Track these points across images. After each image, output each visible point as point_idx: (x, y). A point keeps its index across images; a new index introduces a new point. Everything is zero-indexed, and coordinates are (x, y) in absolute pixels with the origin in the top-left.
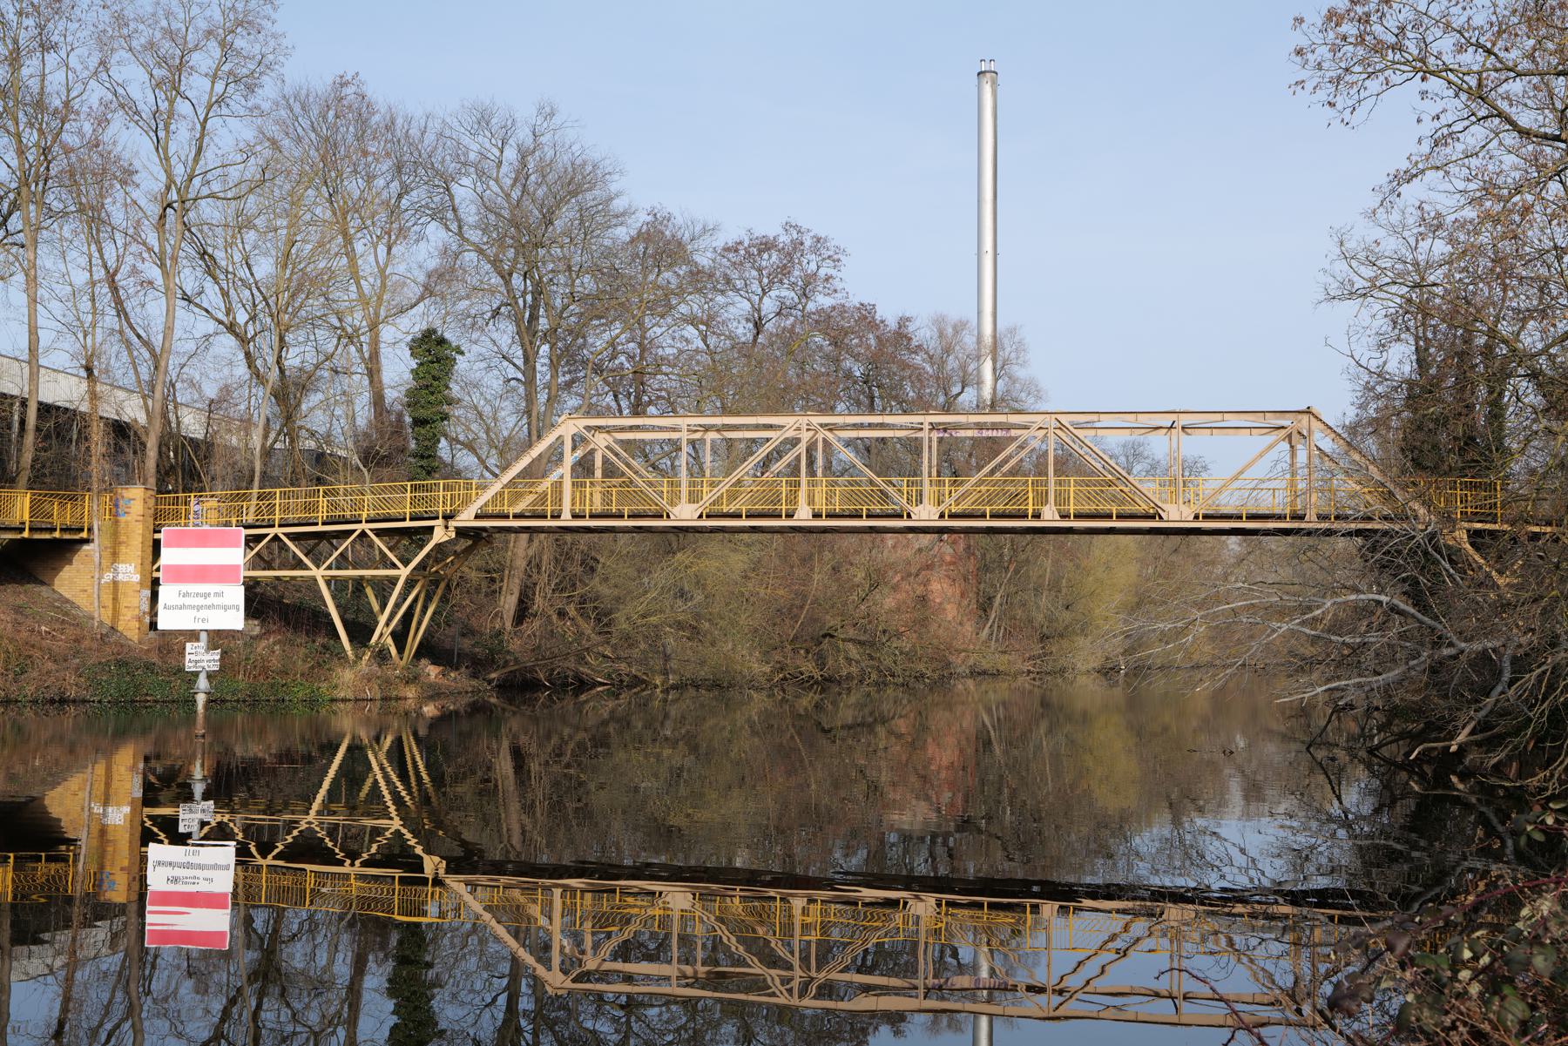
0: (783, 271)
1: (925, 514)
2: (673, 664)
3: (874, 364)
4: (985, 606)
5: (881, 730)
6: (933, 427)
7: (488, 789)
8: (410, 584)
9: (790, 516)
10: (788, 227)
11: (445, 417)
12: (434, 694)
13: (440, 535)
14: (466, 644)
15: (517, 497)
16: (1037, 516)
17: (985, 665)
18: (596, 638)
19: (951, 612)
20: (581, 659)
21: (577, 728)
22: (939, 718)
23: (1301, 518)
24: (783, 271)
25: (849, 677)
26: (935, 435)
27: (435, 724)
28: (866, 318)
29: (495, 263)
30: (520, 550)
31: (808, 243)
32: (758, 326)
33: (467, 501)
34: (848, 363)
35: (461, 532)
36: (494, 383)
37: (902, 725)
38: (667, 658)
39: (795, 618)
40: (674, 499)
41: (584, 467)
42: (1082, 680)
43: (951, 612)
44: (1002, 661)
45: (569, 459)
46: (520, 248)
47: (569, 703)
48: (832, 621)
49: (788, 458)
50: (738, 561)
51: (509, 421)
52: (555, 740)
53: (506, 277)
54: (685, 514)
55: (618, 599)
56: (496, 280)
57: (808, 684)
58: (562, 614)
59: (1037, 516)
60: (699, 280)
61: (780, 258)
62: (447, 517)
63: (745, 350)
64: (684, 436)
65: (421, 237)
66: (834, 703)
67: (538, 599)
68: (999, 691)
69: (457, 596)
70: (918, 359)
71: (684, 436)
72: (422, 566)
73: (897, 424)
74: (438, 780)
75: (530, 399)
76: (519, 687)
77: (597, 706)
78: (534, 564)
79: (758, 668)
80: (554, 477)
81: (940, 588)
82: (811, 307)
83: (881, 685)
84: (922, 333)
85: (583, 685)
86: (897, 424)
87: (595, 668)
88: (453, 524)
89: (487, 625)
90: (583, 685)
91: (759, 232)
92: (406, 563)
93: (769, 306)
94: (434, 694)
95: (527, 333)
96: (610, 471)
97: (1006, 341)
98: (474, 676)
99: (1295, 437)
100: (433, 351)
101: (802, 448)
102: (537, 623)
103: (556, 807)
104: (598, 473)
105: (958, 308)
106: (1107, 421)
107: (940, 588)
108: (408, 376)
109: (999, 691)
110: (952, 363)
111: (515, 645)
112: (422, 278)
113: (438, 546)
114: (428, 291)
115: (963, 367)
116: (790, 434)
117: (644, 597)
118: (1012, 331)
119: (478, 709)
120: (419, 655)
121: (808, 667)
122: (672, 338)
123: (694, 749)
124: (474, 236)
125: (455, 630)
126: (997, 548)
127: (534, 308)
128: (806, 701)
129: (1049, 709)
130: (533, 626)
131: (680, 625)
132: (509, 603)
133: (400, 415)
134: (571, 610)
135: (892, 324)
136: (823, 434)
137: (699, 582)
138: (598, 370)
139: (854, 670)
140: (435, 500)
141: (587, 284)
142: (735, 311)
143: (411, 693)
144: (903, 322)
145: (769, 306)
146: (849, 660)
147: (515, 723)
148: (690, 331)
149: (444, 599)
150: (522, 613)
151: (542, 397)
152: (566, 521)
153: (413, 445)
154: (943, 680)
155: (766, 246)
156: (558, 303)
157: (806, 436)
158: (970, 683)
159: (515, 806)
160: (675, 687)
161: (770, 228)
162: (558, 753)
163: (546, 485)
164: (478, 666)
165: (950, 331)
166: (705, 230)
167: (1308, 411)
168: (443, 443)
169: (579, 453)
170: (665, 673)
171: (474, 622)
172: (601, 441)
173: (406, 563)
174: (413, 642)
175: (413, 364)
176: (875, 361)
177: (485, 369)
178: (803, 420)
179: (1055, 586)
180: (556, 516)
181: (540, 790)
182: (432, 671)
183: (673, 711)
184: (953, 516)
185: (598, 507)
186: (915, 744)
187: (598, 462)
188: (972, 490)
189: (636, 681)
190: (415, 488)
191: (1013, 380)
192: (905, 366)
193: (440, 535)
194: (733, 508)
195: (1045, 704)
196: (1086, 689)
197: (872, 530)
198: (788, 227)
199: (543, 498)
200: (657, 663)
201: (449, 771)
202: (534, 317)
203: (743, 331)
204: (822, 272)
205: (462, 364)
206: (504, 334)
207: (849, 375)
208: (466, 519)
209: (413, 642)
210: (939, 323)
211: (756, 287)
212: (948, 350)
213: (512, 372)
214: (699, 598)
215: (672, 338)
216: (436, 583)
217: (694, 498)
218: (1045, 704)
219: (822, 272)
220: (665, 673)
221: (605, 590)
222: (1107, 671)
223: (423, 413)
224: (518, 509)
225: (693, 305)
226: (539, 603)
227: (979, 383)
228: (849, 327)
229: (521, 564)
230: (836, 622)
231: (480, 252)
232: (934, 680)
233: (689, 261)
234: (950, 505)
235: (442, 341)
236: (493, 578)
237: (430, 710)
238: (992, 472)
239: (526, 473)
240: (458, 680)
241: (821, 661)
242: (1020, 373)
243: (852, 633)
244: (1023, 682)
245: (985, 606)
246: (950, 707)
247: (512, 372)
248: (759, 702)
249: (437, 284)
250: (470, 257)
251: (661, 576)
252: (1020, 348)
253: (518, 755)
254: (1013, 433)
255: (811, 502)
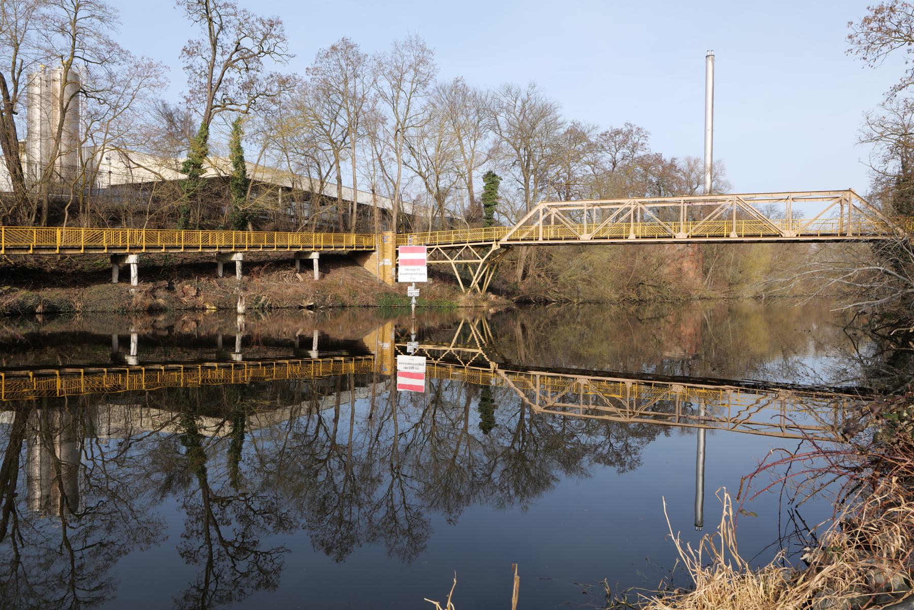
0: (625, 142)
1: (681, 236)
2: (581, 294)
3: (662, 177)
4: (705, 272)
5: (662, 320)
6: (685, 202)
7: (512, 340)
8: (484, 265)
9: (626, 238)
10: (627, 124)
11: (496, 204)
12: (493, 305)
13: (495, 247)
14: (504, 287)
15: (523, 232)
16: (728, 236)
17: (705, 295)
18: (552, 285)
19: (691, 274)
20: (546, 292)
21: (545, 318)
22: (686, 316)
23: (845, 235)
24: (625, 142)
25: (650, 300)
26: (686, 205)
27: (493, 316)
28: (658, 159)
29: (514, 145)
30: (524, 252)
31: (634, 130)
32: (614, 164)
33: (504, 235)
34: (650, 177)
35: (502, 246)
36: (513, 190)
37: (671, 318)
38: (579, 292)
39: (628, 277)
40: (581, 232)
41: (547, 221)
42: (746, 301)
43: (691, 274)
44: (713, 294)
45: (542, 218)
46: (523, 139)
47: (542, 308)
48: (643, 278)
49: (626, 215)
50: (606, 255)
51: (519, 205)
52: (537, 322)
53: (518, 150)
54: (585, 238)
55: (560, 270)
56: (514, 151)
57: (633, 302)
58: (539, 276)
59: (728, 236)
60: (591, 147)
61: (622, 137)
62: (497, 241)
63: (609, 174)
64: (585, 208)
65: (486, 137)
66: (644, 310)
67: (530, 270)
68: (711, 305)
69: (501, 269)
70: (679, 175)
71: (585, 208)
72: (488, 259)
73: (670, 201)
74: (495, 335)
75: (527, 196)
76: (524, 303)
77: (552, 310)
78: (529, 257)
79: (614, 296)
80: (536, 225)
81: (687, 265)
82: (636, 156)
83: (662, 303)
84: (681, 164)
85: (547, 302)
86: (670, 201)
87: (551, 296)
88: (499, 243)
89: (512, 280)
90: (547, 302)
91: (615, 127)
92: (483, 257)
93: (619, 156)
94: (493, 305)
95: (526, 171)
96: (557, 222)
97: (716, 166)
98: (507, 299)
99: (843, 201)
100: (491, 179)
101: (631, 212)
102: (530, 279)
103: (538, 346)
104: (553, 223)
105: (695, 152)
106: (759, 197)
107: (687, 265)
108: (482, 189)
109: (711, 305)
110: (693, 176)
111: (522, 287)
112: (487, 152)
113: (494, 251)
114: (489, 157)
115: (698, 177)
116: (627, 206)
117: (571, 270)
118: (719, 162)
119: (508, 310)
120: (487, 291)
121: (634, 296)
122: (581, 170)
123: (589, 326)
124: (506, 135)
125: (500, 282)
126: (711, 249)
127: (528, 161)
128: (632, 309)
129: (732, 312)
130: (528, 280)
131: (584, 280)
132: (520, 272)
133: (480, 204)
134: (543, 274)
135: (669, 161)
136: (640, 206)
137: (591, 264)
138: (552, 184)
139: (652, 297)
140: (492, 235)
141: (548, 151)
142: (605, 159)
143: (485, 304)
144: (673, 160)
145: (619, 156)
146: (650, 293)
147: (522, 316)
148: (588, 168)
149: (496, 271)
150: (524, 276)
151: (531, 195)
152: (541, 241)
153: (484, 214)
154: (688, 301)
155: (618, 132)
156: (537, 159)
157: (633, 207)
158: (699, 302)
159: (522, 346)
160: (582, 303)
161: (620, 125)
162: (538, 327)
163: (533, 228)
164: (509, 295)
165: (692, 163)
166: (593, 128)
167: (850, 190)
168: (495, 213)
169: (545, 216)
170: (578, 298)
171: (507, 279)
172: (553, 211)
173: (483, 257)
174: (485, 286)
175: (484, 184)
176: (661, 176)
177: (511, 185)
178: (632, 201)
179: (735, 264)
180: (537, 240)
181: (532, 338)
182: (492, 297)
183: (581, 312)
184: (692, 237)
185: (553, 236)
186: (676, 326)
187: (553, 219)
188: (701, 227)
189: (567, 301)
190: (485, 230)
191: (719, 181)
192: (674, 177)
193: (495, 247)
194: (604, 235)
195: (730, 310)
196: (747, 304)
197: (659, 243)
198: (627, 124)
199: (532, 233)
200: (575, 294)
201: (499, 333)
202: (528, 165)
203: (609, 166)
204: (640, 142)
205: (502, 183)
206: (517, 171)
207: (651, 182)
208: (504, 241)
209: (485, 286)
210: (688, 160)
211: (613, 149)
212: (692, 170)
213: (520, 186)
214: (591, 269)
215: (581, 170)
216: (493, 265)
217: (589, 232)
218: (730, 310)
219: (640, 142)
220: (578, 298)
221: (555, 267)
222: (757, 298)
223: (488, 203)
224: (523, 237)
225: (589, 157)
226: (531, 272)
227: (705, 183)
228: (649, 163)
229: (524, 257)
230: (645, 278)
231: (508, 141)
232: (684, 301)
233: (587, 140)
234: (691, 232)
235: (494, 176)
236: (514, 262)
237: (492, 311)
238: (710, 219)
239: (525, 224)
240: (502, 300)
241: (639, 294)
242: (722, 178)
243: (651, 283)
244: (721, 302)
245: (705, 272)
246: (690, 311)
247: (520, 186)
248: (614, 308)
249: (493, 154)
250: (505, 143)
251: (576, 262)
252: (722, 168)
253: (523, 327)
254: (719, 203)
255: (635, 232)
